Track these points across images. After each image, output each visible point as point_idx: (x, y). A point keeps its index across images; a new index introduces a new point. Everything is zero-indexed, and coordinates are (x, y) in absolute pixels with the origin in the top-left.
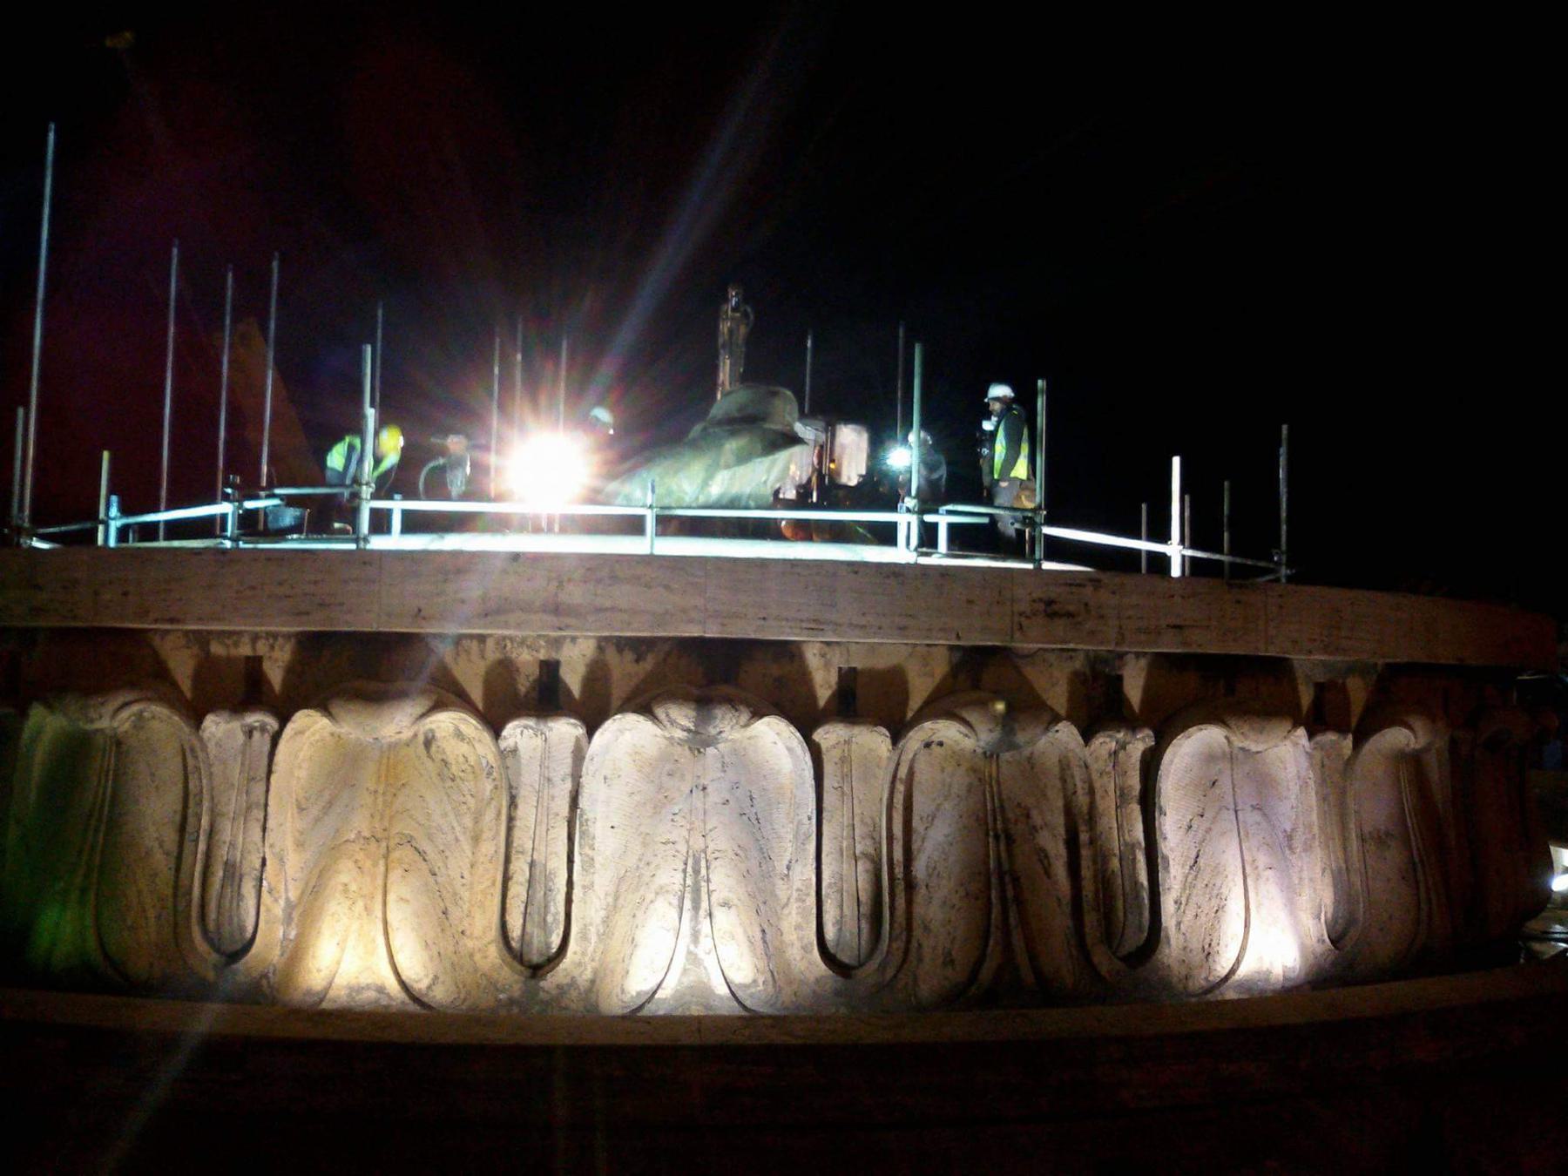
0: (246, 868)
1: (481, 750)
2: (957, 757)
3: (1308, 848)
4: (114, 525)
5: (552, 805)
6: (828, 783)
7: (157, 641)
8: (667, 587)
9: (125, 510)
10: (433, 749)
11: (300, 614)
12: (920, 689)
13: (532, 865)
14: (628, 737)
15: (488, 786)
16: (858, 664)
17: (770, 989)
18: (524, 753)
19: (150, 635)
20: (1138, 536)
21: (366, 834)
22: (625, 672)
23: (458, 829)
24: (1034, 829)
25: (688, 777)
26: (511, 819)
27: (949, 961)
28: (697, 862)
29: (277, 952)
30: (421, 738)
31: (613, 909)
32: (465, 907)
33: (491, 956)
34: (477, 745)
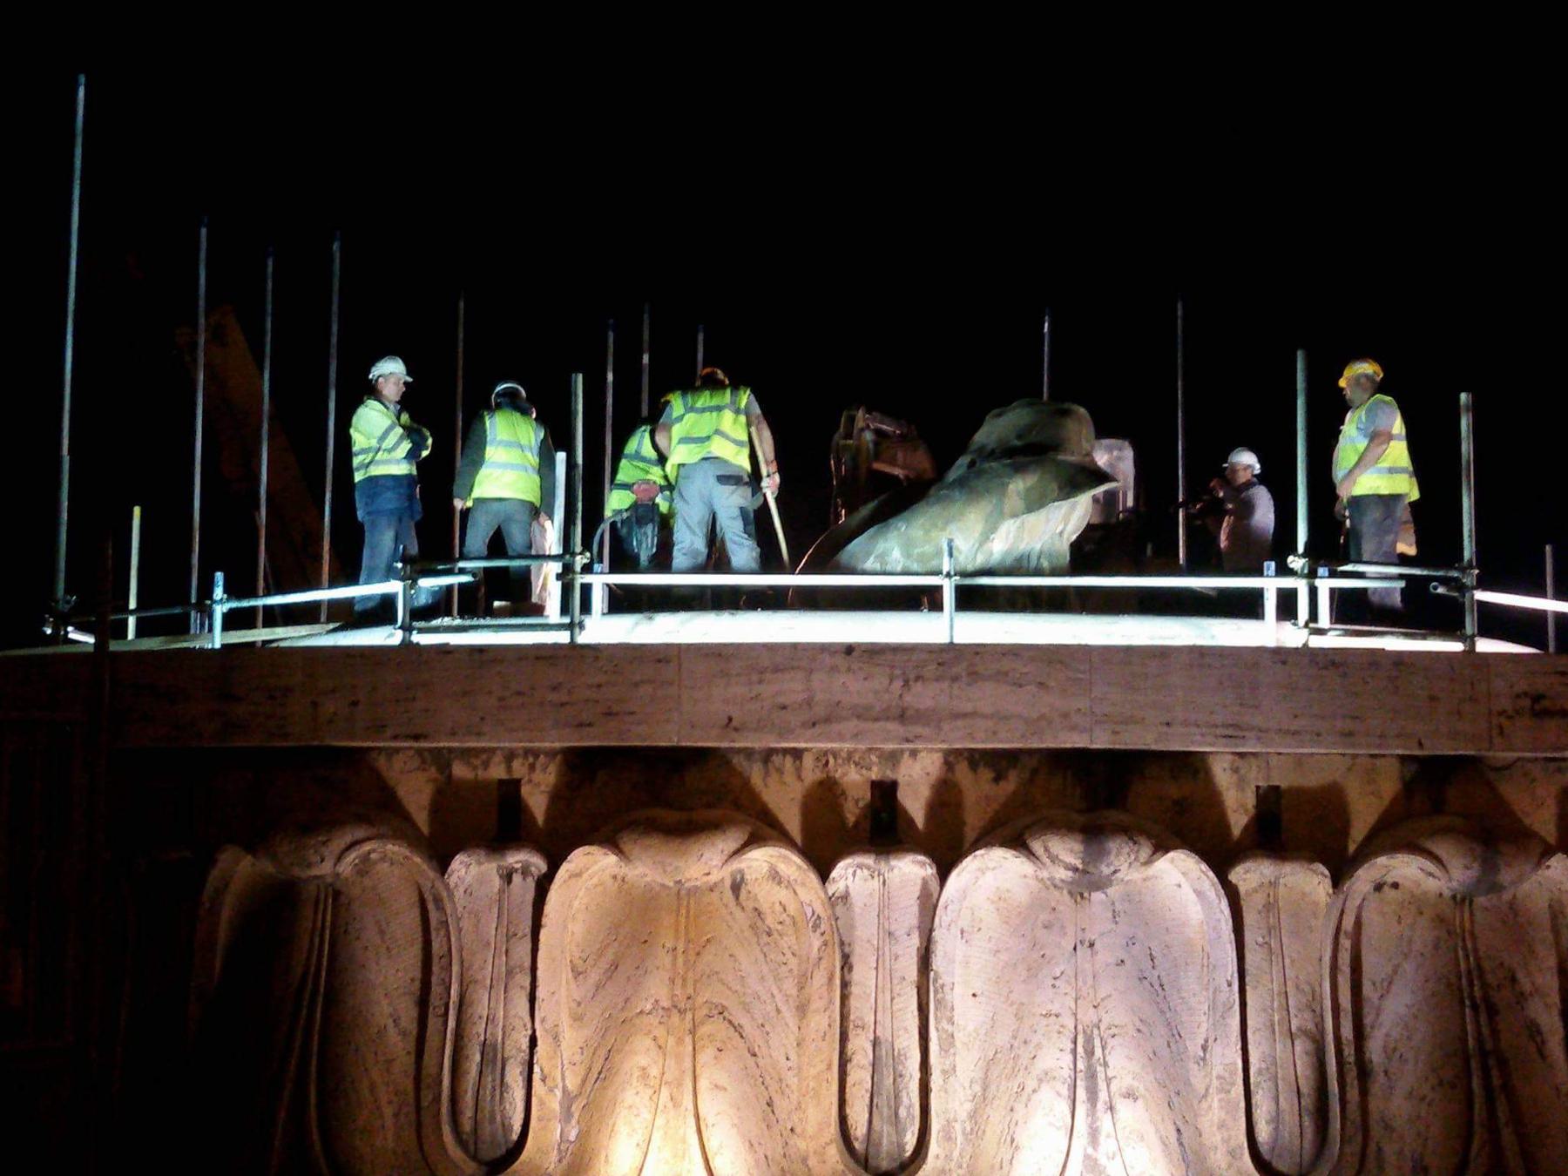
0: (510, 1050)
1: (804, 895)
2: (1418, 903)
4: (219, 611)
5: (897, 966)
6: (1250, 937)
7: (381, 762)
9: (232, 591)
11: (581, 725)
12: (1363, 816)
13: (875, 1043)
14: (992, 877)
16: (1283, 780)
18: (857, 899)
19: (374, 755)
20: (1540, 592)
21: (666, 1003)
23: (778, 997)
24: (1521, 998)
25: (1071, 930)
26: (845, 985)
28: (1089, 1040)
29: (554, 1156)
30: (728, 883)
31: (983, 1099)
32: (794, 1097)
34: (799, 890)
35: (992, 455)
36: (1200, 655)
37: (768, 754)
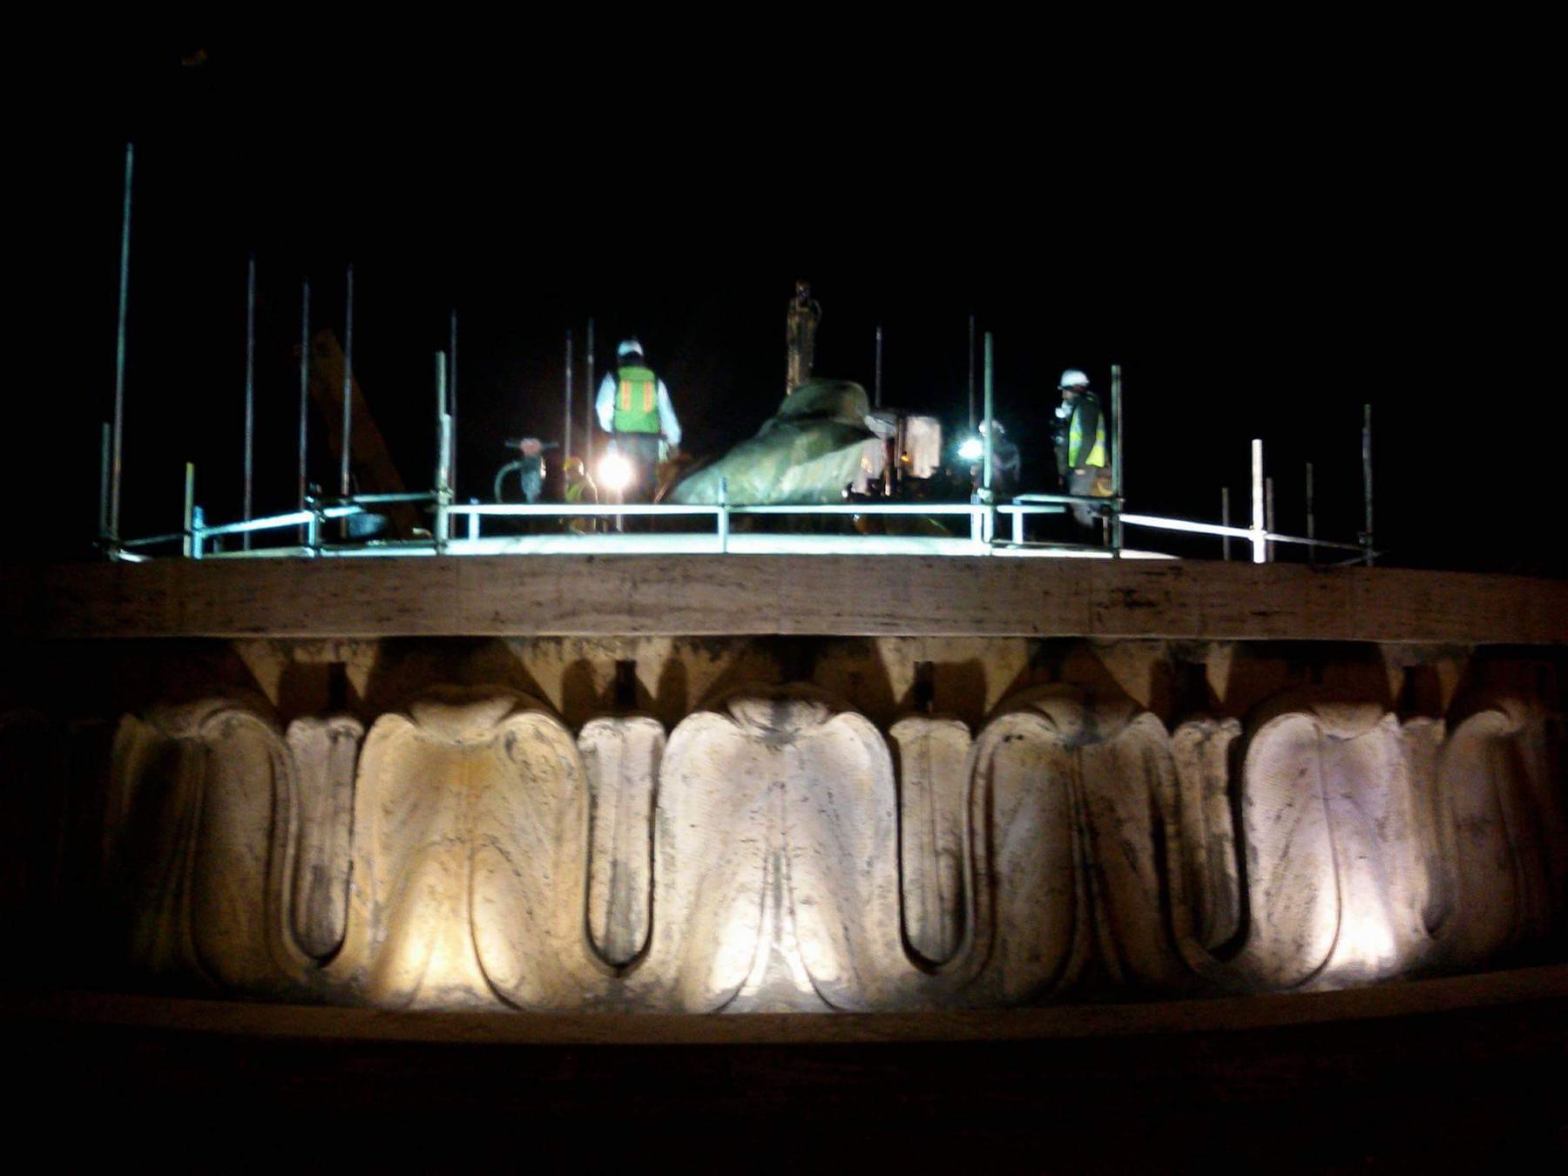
0: (334, 873)
1: (561, 750)
2: (1038, 751)
3: (1400, 836)
6: (908, 778)
7: (242, 649)
8: (740, 585)
9: (210, 521)
10: (515, 751)
12: (998, 682)
13: (614, 864)
14: (704, 734)
15: (569, 786)
16: (936, 656)
17: (855, 986)
18: (603, 752)
20: (1219, 522)
22: (700, 670)
24: (1119, 822)
26: (592, 819)
27: (1035, 957)
28: (777, 859)
30: (502, 740)
31: (696, 906)
33: (575, 955)
35: (789, 419)
36: (929, 561)
37: (536, 642)
